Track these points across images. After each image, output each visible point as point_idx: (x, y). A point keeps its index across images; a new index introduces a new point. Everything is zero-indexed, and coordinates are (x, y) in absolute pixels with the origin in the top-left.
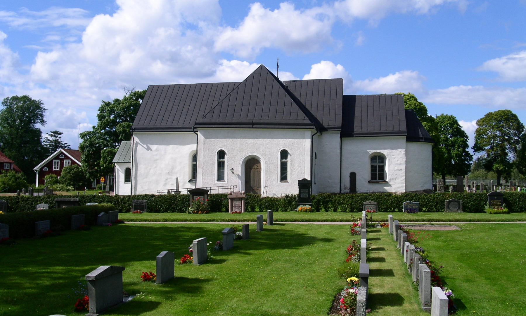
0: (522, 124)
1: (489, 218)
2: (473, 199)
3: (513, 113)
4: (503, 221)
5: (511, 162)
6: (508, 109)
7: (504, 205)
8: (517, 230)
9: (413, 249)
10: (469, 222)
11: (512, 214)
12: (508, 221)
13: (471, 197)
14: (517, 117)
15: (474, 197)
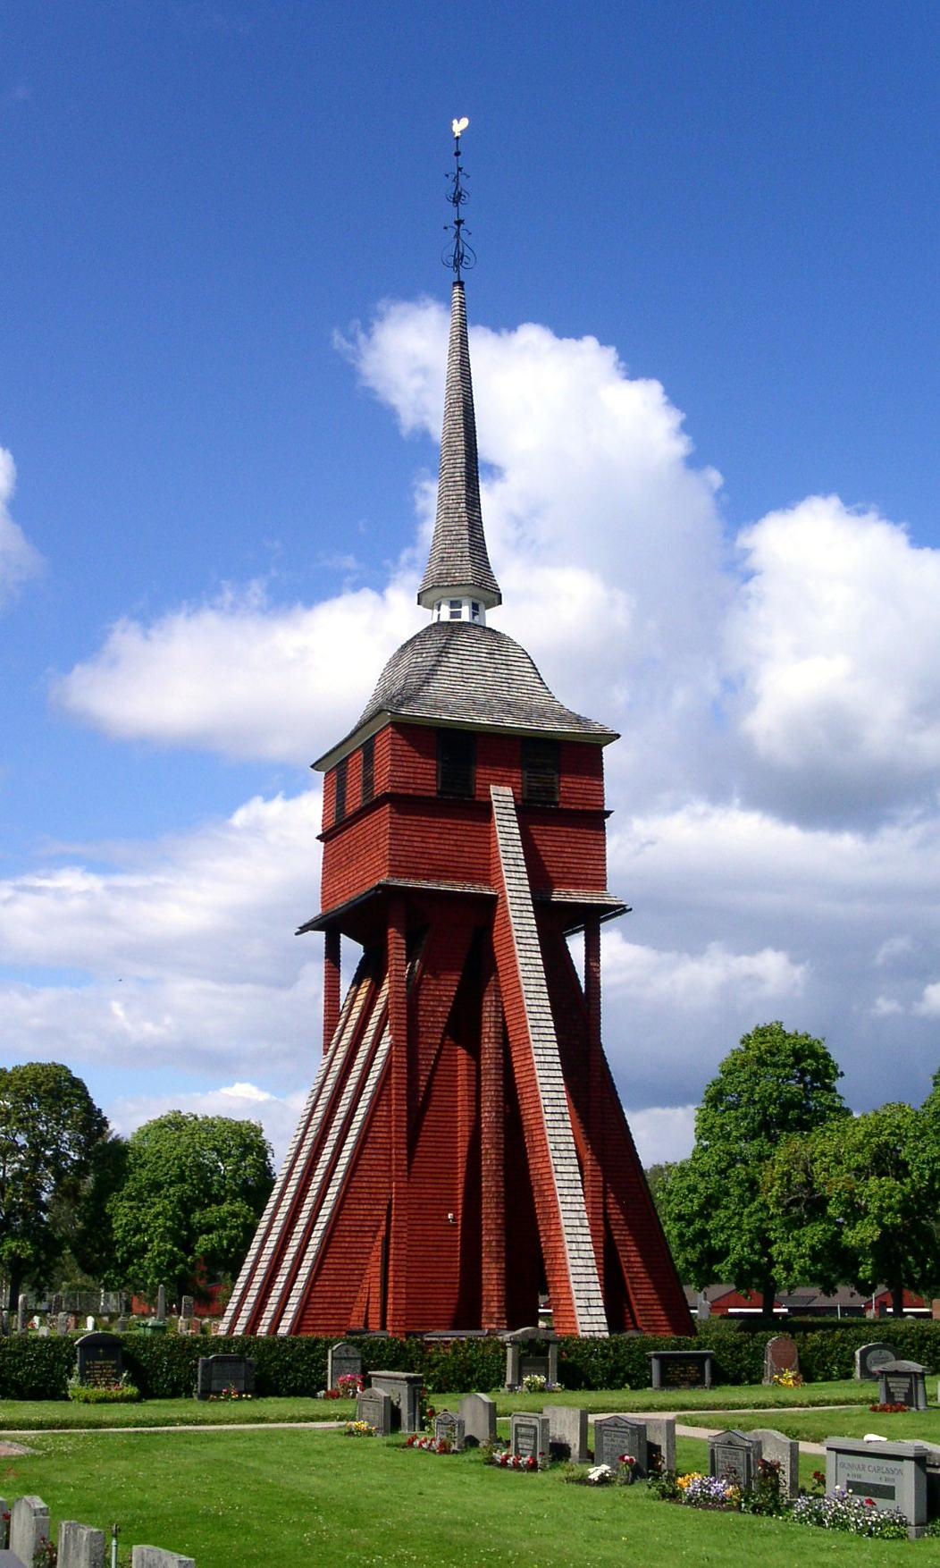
0: (100, 1110)
1: (97, 1417)
2: (31, 1356)
3: (75, 1075)
4: (138, 1423)
5: (695, 1261)
6: (59, 1061)
7: (125, 1375)
8: (216, 1451)
9: (41, 1509)
10: (38, 1429)
11: (149, 1402)
12: (153, 1426)
13: (26, 1349)
14: (84, 1088)
15: (34, 1349)
